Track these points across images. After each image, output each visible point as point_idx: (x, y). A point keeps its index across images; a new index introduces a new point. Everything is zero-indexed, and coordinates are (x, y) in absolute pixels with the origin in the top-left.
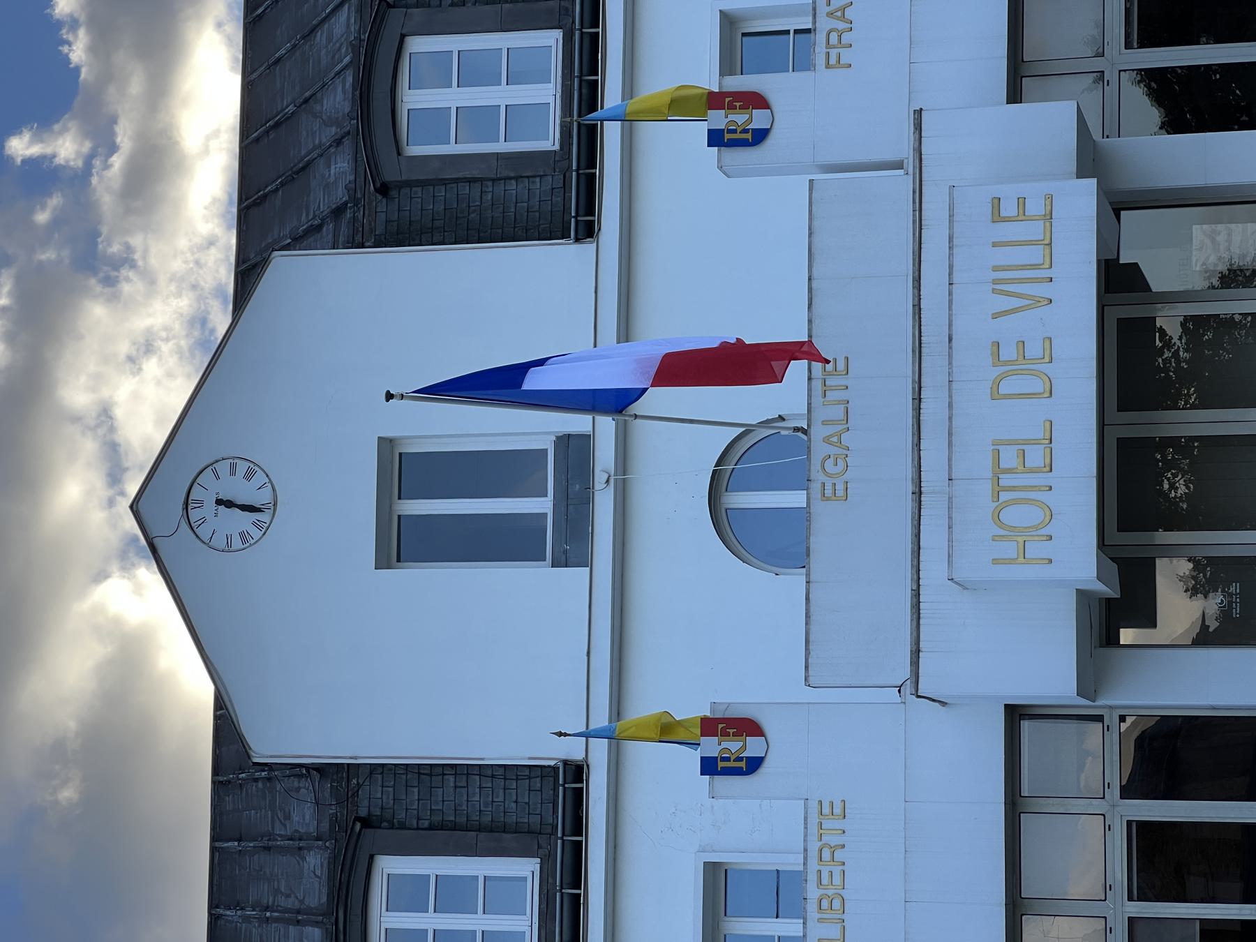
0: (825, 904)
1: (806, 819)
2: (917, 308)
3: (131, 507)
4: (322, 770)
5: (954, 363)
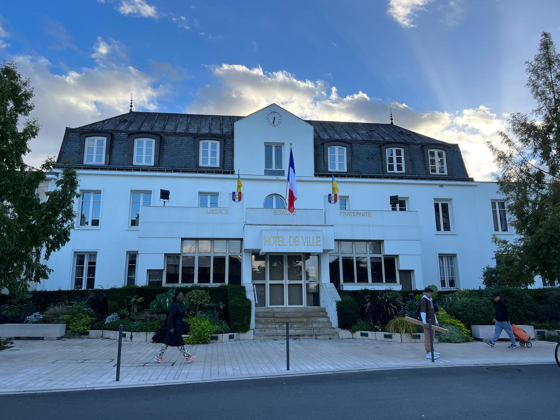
3: (274, 104)
4: (233, 133)
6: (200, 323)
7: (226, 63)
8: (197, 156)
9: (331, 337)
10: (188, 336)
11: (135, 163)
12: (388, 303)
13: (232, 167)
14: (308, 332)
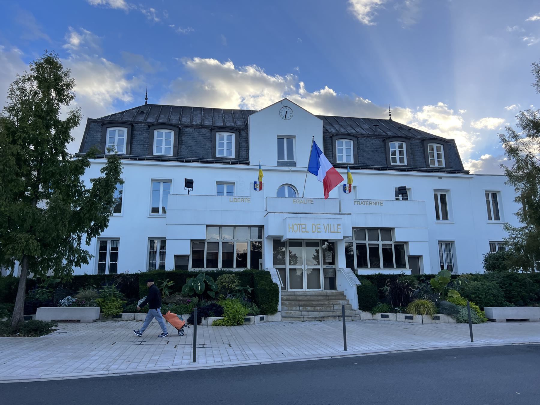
6: (233, 305)
7: (197, 56)
8: (213, 148)
9: (353, 318)
10: (222, 318)
11: (155, 153)
12: (408, 285)
13: (248, 159)
14: (330, 314)
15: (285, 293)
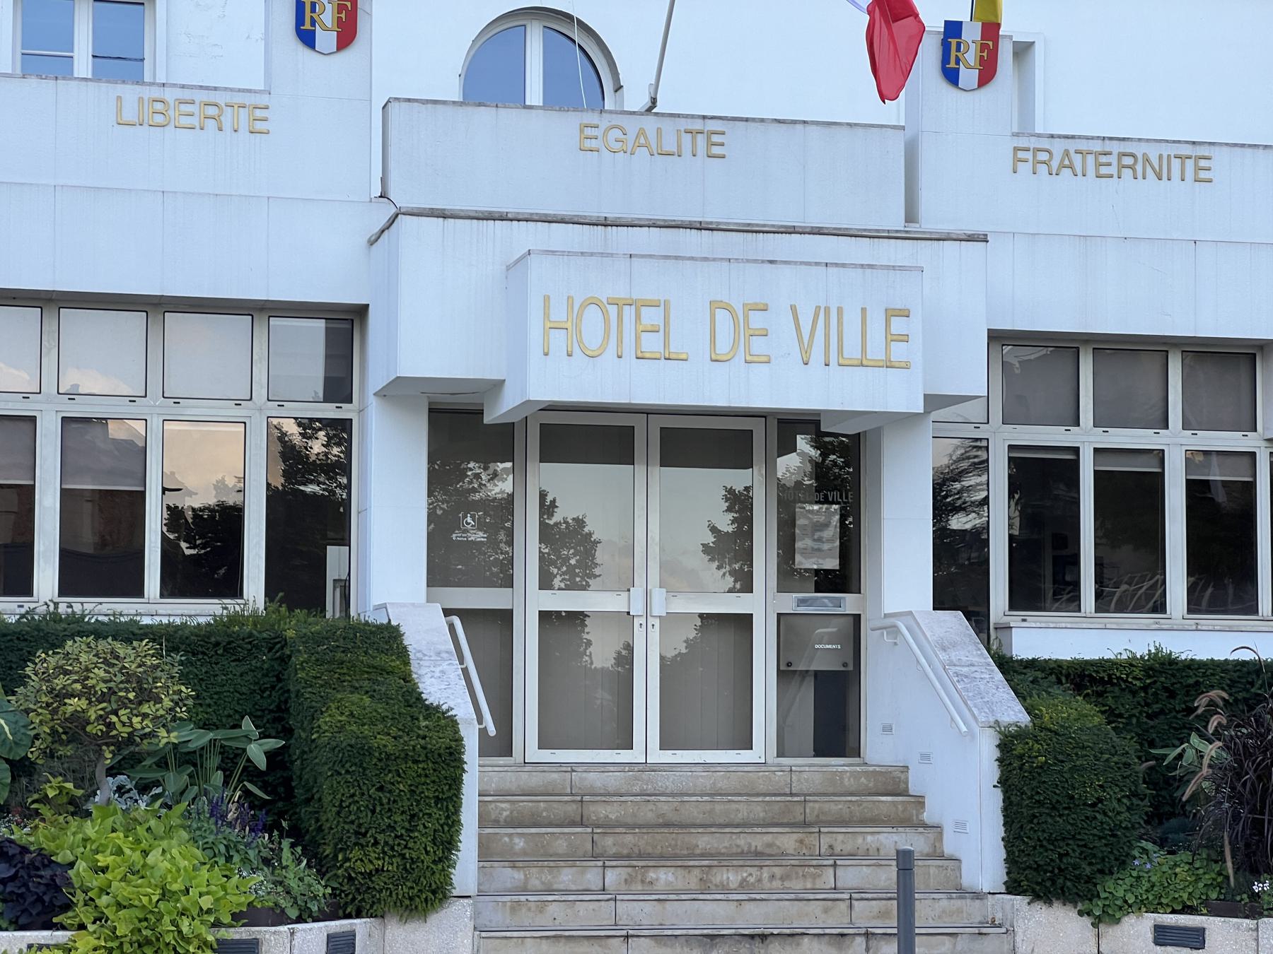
0: (159, 106)
1: (249, 91)
2: (791, 231)
5: (748, 265)
10: (60, 936)
14: (812, 916)
15: (502, 773)
